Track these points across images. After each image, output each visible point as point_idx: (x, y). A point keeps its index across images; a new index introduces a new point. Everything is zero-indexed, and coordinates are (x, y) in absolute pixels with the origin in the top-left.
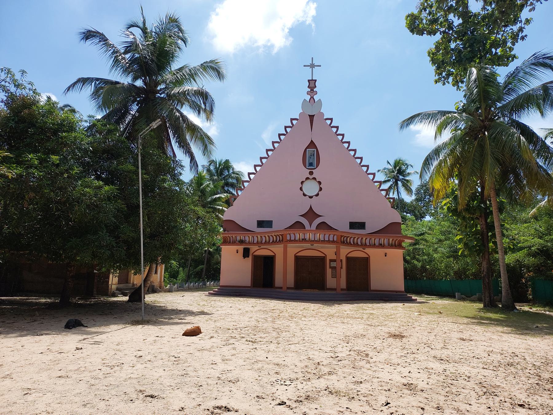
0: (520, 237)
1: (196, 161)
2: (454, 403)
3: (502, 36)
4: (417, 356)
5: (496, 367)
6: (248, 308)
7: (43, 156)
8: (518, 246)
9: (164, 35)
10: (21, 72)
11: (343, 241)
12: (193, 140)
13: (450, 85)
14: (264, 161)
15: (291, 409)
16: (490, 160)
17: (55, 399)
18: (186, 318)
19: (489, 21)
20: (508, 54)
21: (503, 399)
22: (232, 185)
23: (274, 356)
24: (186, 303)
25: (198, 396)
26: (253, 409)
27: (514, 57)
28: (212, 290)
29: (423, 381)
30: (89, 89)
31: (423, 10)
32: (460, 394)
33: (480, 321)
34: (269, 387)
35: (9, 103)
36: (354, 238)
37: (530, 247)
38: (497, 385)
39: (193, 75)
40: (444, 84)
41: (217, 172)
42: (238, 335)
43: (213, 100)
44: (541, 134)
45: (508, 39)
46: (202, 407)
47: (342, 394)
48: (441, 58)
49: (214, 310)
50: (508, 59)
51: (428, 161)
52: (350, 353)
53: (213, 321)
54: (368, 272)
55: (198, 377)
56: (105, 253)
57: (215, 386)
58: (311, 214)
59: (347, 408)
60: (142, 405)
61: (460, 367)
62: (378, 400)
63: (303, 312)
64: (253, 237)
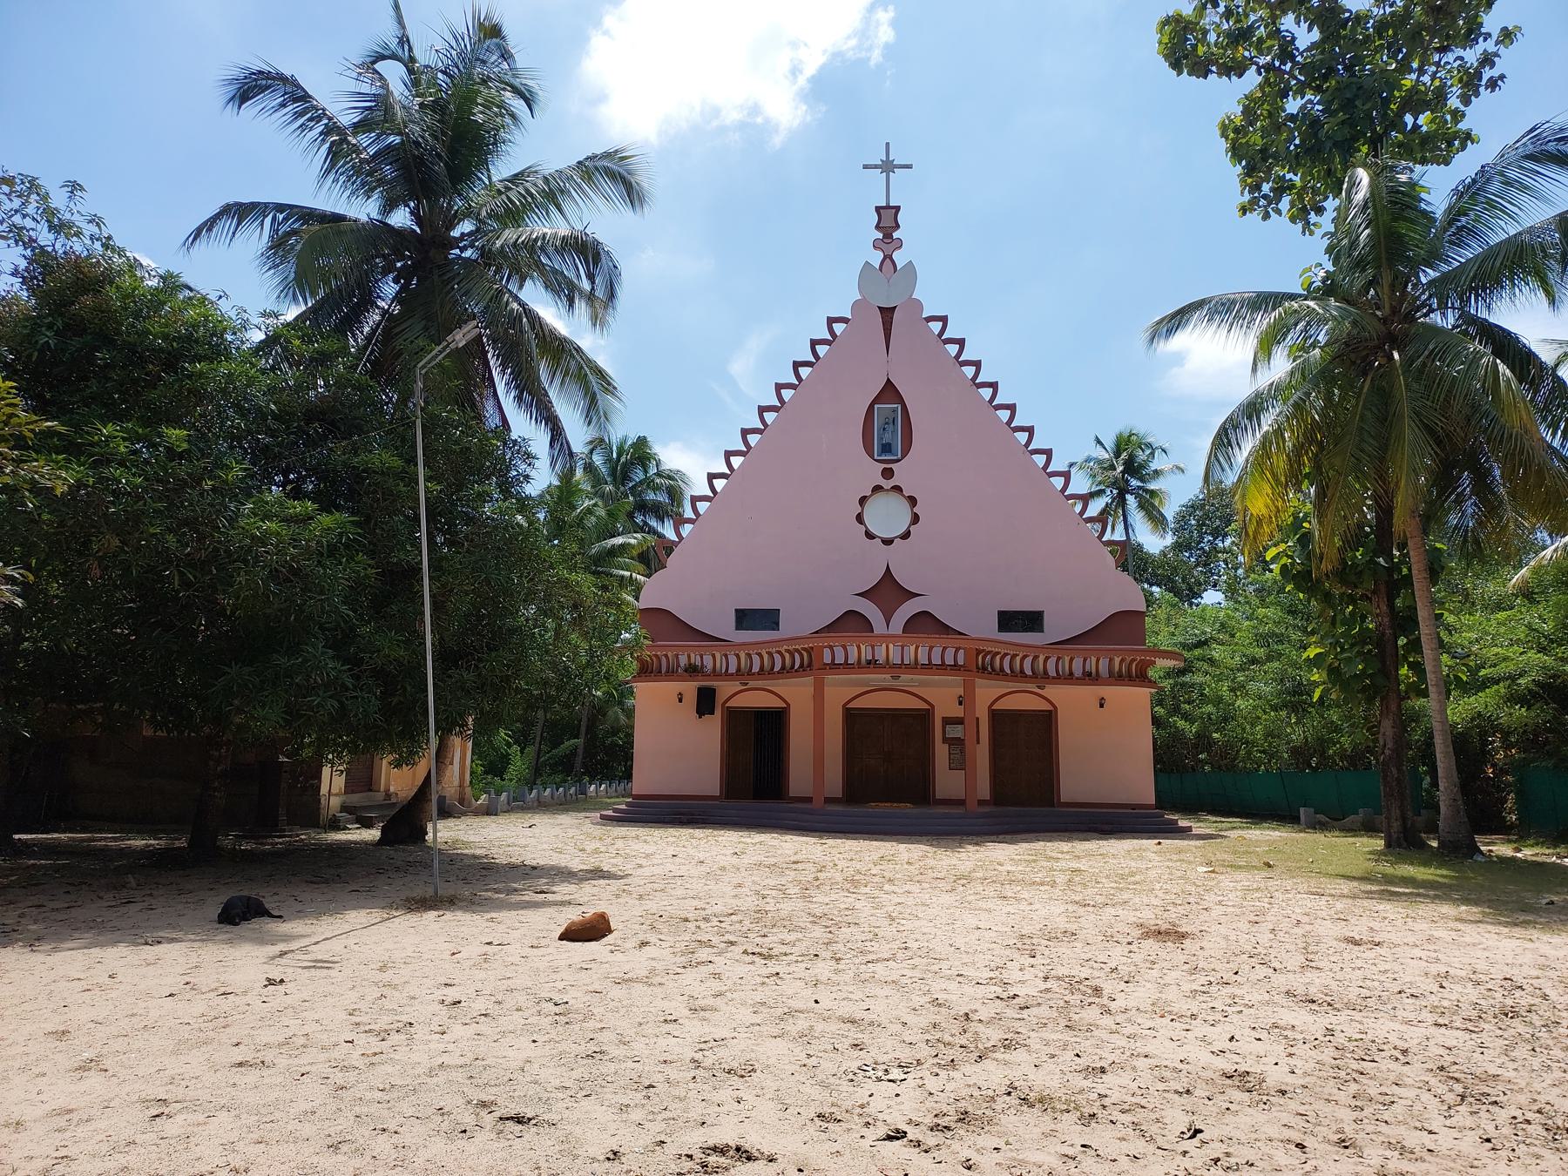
0: (1485, 651)
1: (568, 443)
2: (1383, 1128)
3: (1433, 77)
4: (1238, 992)
5: (1470, 1020)
6: (724, 858)
7: (140, 431)
8: (1481, 674)
9: (470, 76)
10: (68, 186)
11: (982, 665)
12: (557, 381)
13: (1285, 219)
14: (753, 439)
15: (926, 1152)
16: (1409, 431)
17: (245, 1129)
18: (554, 889)
19: (1395, 34)
20: (1449, 129)
21: (1518, 1113)
22: (659, 512)
23: (834, 996)
24: (545, 846)
25: (651, 1117)
26: (818, 1153)
27: (1468, 137)
28: (606, 806)
29: (1276, 1064)
30: (254, 239)
31: (1209, 6)
32: (1393, 1102)
33: (1388, 887)
34: (845, 1086)
35: (36, 278)
36: (1014, 656)
37: (1512, 678)
38: (1490, 1073)
39: (553, 195)
40: (1266, 216)
41: (613, 472)
42: (717, 937)
43: (615, 267)
44: (1547, 355)
45: (1450, 87)
46: (671, 1149)
47: (1059, 1106)
48: (1260, 142)
49: (629, 866)
50: (1450, 144)
51: (1227, 435)
52: (1048, 985)
53: (634, 896)
54: (1051, 752)
55: (636, 1059)
56: (323, 706)
57: (691, 1085)
58: (888, 591)
59: (1083, 1146)
60: (496, 1144)
61: (1369, 1023)
62: (1165, 1121)
63: (882, 867)
64: (726, 656)
